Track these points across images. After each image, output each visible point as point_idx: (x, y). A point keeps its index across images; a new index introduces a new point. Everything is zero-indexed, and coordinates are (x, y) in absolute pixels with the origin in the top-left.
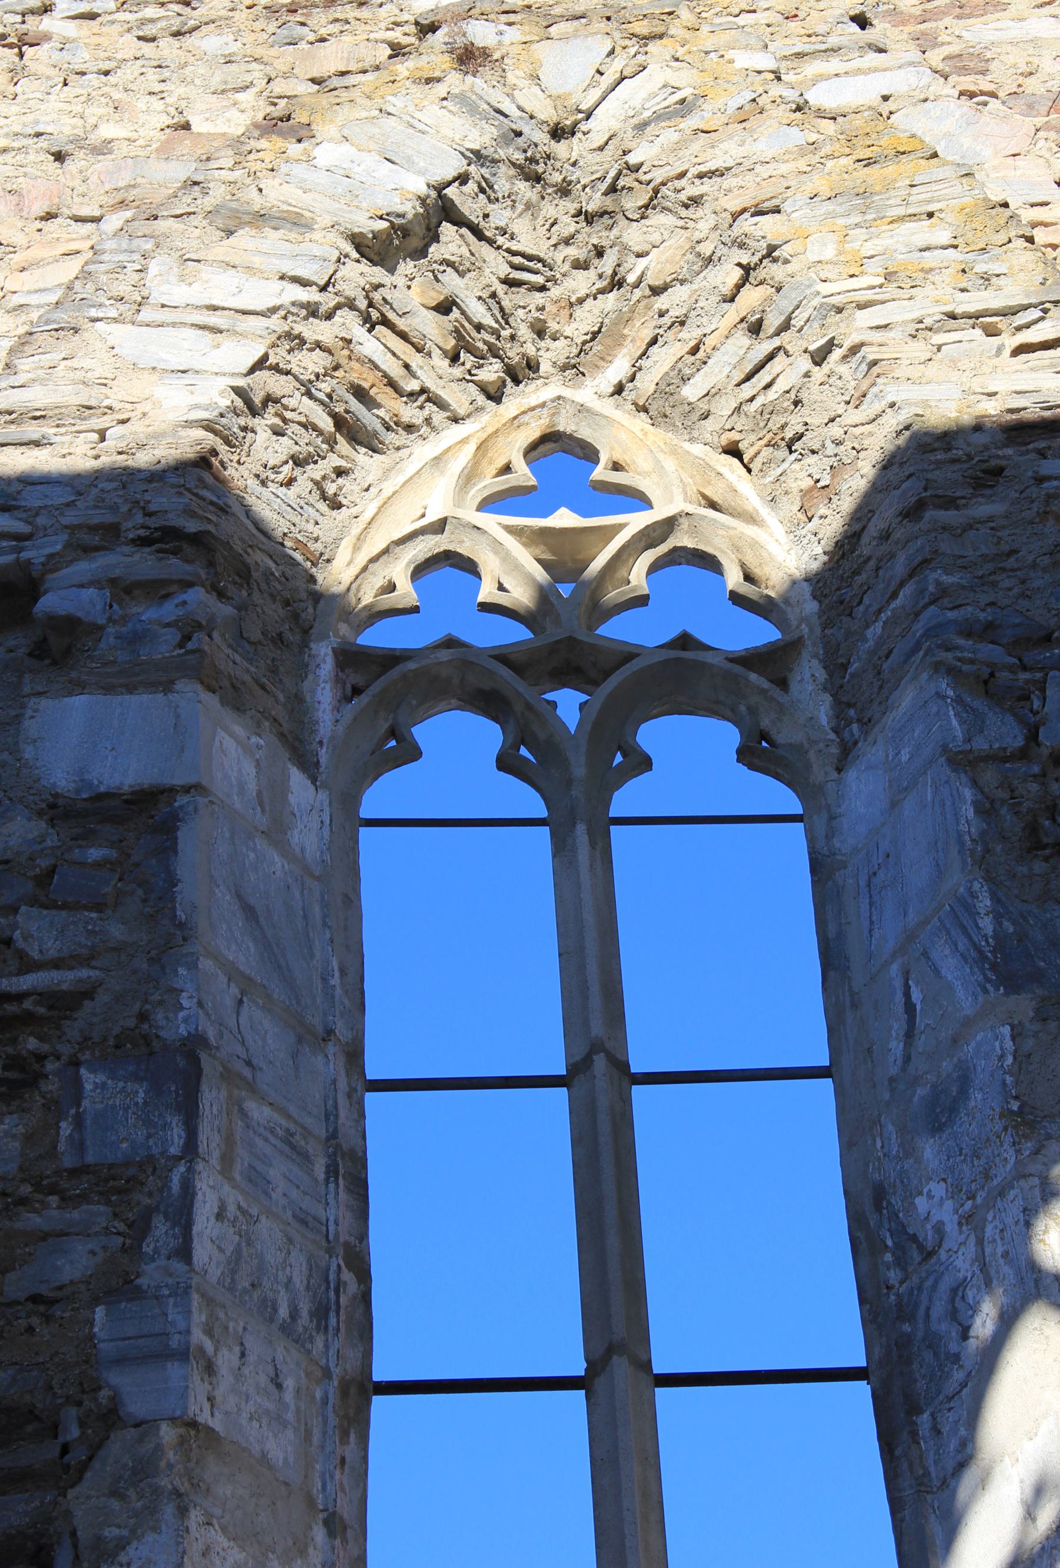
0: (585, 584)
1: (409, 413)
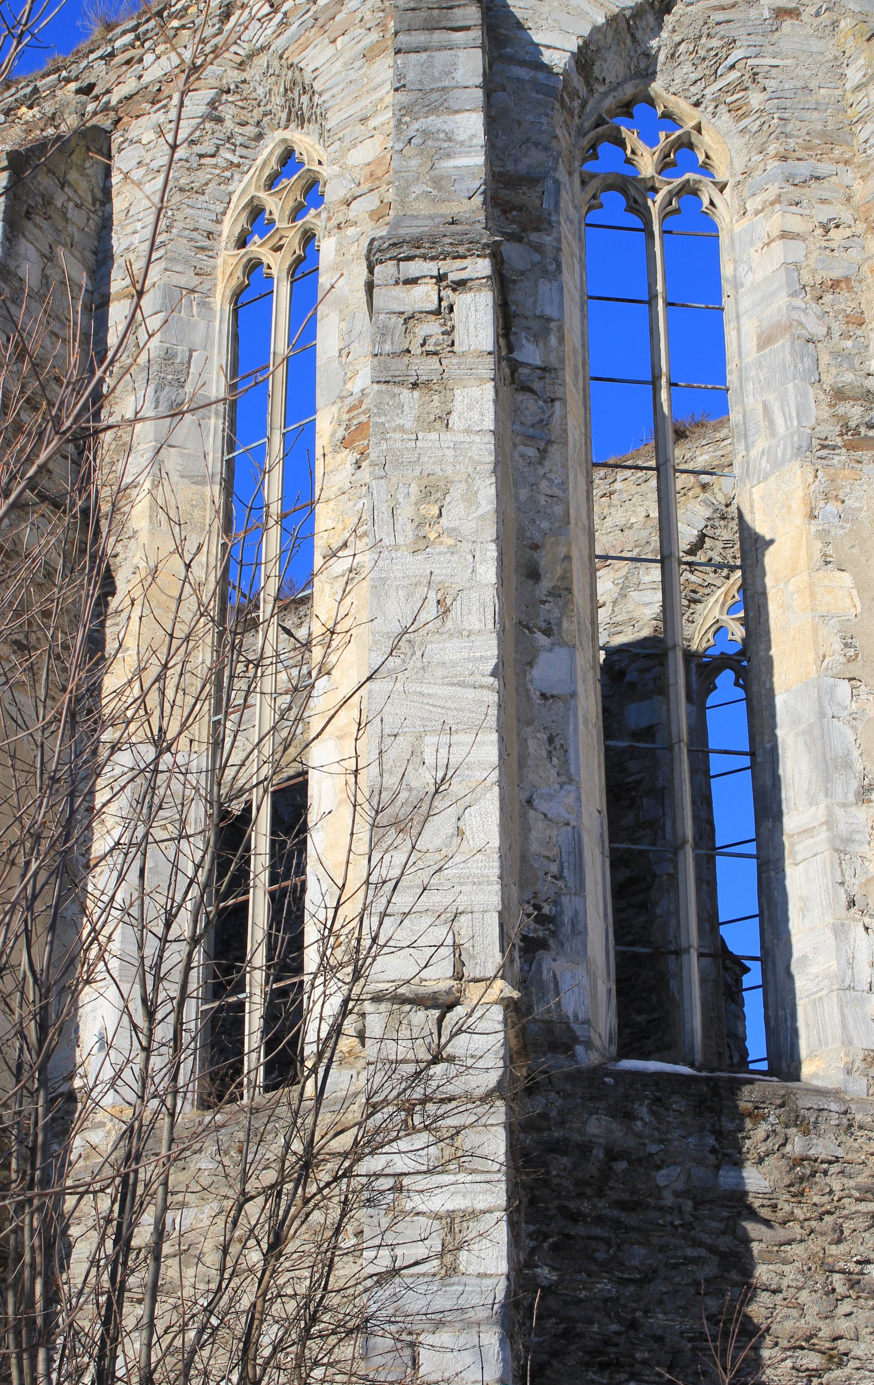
0: (7, 1289)
1: (707, 591)
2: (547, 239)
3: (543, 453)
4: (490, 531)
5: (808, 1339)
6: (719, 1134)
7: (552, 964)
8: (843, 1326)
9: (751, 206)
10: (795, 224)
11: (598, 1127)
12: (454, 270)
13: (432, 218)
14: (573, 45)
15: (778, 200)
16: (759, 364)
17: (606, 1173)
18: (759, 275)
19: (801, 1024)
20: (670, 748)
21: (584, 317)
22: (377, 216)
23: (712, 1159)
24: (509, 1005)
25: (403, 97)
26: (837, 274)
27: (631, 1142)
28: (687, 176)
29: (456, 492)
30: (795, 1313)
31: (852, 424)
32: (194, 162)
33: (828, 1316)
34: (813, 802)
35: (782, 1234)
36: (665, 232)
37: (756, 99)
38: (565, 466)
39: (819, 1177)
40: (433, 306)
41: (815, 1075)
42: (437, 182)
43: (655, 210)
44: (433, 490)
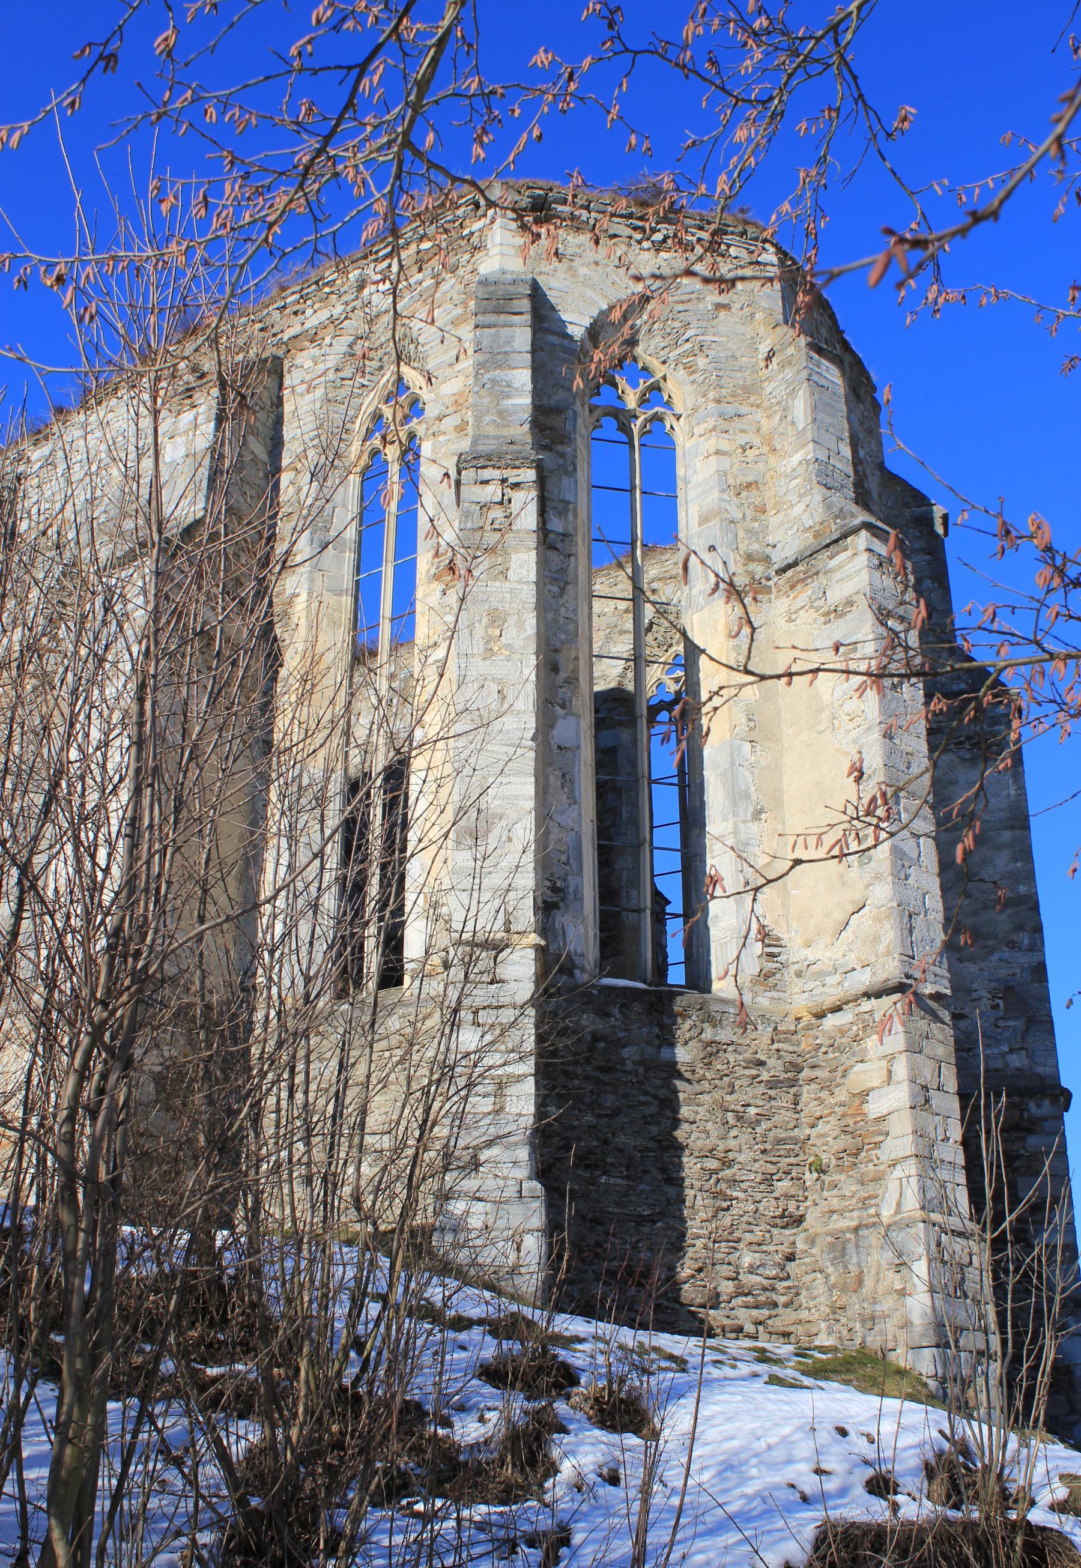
2: (568, 450)
3: (563, 590)
4: (532, 647)
5: (711, 1151)
6: (662, 1026)
7: (561, 919)
8: (732, 1143)
9: (697, 431)
10: (724, 445)
11: (589, 1022)
12: (513, 476)
13: (497, 438)
14: (587, 322)
15: (714, 429)
16: (699, 536)
17: (592, 1049)
18: (700, 477)
19: (713, 958)
20: (637, 781)
21: (589, 499)
22: (461, 429)
23: (656, 1041)
24: (537, 948)
25: (480, 357)
26: (750, 479)
27: (608, 1031)
28: (657, 409)
29: (511, 621)
30: (703, 1135)
31: (757, 577)
32: (338, 383)
33: (724, 1138)
34: (725, 819)
35: (697, 1088)
36: (641, 445)
37: (701, 362)
38: (576, 599)
39: (721, 1054)
40: (498, 499)
41: (721, 990)
42: (501, 414)
43: (636, 431)
44: (496, 618)
